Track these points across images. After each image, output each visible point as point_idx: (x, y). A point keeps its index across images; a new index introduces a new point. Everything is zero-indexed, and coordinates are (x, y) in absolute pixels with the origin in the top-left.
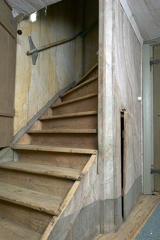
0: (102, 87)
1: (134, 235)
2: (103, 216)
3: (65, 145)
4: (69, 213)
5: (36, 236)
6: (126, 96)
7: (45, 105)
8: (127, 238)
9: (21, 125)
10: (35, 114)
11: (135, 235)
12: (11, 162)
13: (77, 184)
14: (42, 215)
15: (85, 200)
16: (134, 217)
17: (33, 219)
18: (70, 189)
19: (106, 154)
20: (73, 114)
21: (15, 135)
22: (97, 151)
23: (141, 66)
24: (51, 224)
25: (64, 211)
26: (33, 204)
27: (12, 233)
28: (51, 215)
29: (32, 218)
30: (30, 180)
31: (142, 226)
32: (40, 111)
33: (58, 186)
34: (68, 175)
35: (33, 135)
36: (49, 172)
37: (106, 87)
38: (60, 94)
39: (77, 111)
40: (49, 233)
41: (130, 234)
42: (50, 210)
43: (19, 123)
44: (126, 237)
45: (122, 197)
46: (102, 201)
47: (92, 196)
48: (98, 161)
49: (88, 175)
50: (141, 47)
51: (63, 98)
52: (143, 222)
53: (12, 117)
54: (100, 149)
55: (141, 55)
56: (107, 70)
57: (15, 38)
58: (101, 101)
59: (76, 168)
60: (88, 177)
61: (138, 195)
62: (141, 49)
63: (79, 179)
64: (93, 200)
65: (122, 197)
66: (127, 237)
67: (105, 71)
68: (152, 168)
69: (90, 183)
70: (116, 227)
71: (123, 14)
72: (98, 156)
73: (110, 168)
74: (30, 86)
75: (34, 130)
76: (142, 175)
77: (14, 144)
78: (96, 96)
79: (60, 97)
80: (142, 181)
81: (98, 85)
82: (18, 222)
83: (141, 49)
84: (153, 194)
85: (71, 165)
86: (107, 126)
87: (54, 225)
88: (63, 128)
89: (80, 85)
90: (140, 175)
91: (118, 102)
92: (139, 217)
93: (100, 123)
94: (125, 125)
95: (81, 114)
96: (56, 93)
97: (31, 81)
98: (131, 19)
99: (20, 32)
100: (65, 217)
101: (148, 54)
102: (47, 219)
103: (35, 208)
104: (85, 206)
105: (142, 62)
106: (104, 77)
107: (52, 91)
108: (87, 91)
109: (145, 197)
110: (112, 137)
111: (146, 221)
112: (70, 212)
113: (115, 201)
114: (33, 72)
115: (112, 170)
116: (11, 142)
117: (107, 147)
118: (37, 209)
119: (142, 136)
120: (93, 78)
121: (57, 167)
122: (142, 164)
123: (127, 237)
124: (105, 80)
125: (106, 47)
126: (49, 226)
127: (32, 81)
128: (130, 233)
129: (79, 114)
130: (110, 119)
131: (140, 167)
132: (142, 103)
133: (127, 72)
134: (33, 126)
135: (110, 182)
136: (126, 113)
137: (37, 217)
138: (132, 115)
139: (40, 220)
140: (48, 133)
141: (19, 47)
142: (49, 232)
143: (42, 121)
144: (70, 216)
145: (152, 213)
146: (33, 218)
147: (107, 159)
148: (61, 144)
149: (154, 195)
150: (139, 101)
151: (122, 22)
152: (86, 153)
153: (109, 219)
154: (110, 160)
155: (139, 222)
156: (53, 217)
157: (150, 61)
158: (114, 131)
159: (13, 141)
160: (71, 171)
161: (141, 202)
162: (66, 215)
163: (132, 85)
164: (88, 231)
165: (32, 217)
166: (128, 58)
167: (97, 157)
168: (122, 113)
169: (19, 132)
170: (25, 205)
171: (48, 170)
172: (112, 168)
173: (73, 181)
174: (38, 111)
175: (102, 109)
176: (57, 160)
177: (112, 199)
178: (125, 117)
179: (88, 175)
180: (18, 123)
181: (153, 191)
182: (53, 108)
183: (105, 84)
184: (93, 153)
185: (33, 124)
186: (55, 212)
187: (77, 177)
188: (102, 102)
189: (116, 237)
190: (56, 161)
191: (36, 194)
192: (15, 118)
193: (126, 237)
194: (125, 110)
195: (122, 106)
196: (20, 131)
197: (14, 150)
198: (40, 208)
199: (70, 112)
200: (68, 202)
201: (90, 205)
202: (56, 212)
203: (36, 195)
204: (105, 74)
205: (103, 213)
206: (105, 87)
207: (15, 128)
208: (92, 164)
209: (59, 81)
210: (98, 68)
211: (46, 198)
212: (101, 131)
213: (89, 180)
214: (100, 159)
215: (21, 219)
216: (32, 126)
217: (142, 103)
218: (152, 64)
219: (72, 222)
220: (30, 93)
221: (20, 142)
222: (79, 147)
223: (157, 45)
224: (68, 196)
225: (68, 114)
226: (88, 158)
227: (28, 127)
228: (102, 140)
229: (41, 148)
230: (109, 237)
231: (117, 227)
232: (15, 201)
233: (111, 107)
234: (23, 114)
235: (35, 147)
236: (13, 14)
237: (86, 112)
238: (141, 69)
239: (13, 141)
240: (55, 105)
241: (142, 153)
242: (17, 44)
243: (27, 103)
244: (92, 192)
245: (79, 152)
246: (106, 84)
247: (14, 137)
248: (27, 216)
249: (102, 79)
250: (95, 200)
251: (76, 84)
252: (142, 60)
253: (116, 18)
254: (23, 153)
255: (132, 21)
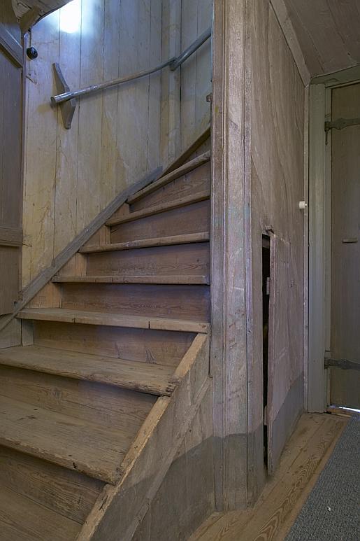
0: (220, 177)
1: (290, 511)
2: (221, 472)
3: (136, 309)
4: (144, 475)
5: (65, 529)
6: (273, 199)
7: (94, 221)
8: (275, 521)
9: (39, 265)
10: (71, 240)
11: (294, 514)
12: (16, 348)
13: (161, 404)
14: (80, 480)
15: (181, 440)
16: (293, 463)
17: (59, 487)
18: (146, 415)
19: (231, 334)
20: (155, 241)
21: (26, 288)
22: (208, 324)
23: (306, 133)
24: (98, 504)
25: (130, 473)
26: (59, 454)
27: (8, 521)
28: (100, 483)
29: (56, 486)
30: (56, 390)
31: (309, 489)
32: (82, 232)
33: (120, 408)
34: (142, 383)
35: (68, 288)
36: (97, 375)
37: (230, 177)
38: (127, 195)
39: (163, 234)
40: (94, 529)
41: (281, 510)
42: (98, 470)
43: (34, 261)
44: (274, 519)
45: (265, 428)
46: (219, 438)
47: (197, 429)
48: (210, 347)
49: (188, 382)
50: (306, 90)
51: (132, 204)
52: (309, 479)
53: (17, 248)
54: (214, 320)
55: (306, 108)
56: (231, 139)
57: (18, 65)
58: (217, 209)
59: (160, 363)
60: (188, 388)
61: (296, 415)
62: (306, 96)
63: (168, 393)
64: (200, 439)
65: (265, 428)
66: (276, 518)
67: (227, 139)
68: (326, 356)
69: (192, 400)
70: (251, 495)
71: (268, 8)
72: (211, 337)
73: (238, 364)
74: (58, 176)
75: (67, 276)
76: (306, 371)
77: (23, 308)
78: (207, 199)
79: (126, 202)
80: (306, 385)
81: (211, 173)
82: (26, 492)
83: (306, 96)
84: (328, 413)
85: (150, 356)
86: (231, 268)
87: (105, 507)
88: (133, 271)
89: (170, 175)
90: (301, 371)
91: (257, 212)
92: (301, 467)
93: (215, 262)
94: (273, 267)
95: (172, 239)
96: (119, 193)
97: (59, 166)
98: (285, 22)
99: (32, 54)
100: (133, 483)
101: (318, 107)
102: (91, 491)
103: (62, 464)
104: (180, 455)
105: (306, 125)
106: (225, 155)
107: (110, 188)
108: (187, 187)
109: (311, 418)
110: (242, 294)
111: (315, 477)
112: (144, 472)
113: (247, 437)
114: (64, 146)
115: (242, 368)
116: (15, 302)
117: (231, 315)
118: (68, 466)
119: (306, 288)
120: (201, 157)
121: (119, 361)
122: (306, 348)
123: (276, 518)
124: (227, 161)
125: (231, 84)
126: (93, 512)
127: (63, 165)
128: (283, 507)
129: (168, 239)
130: (238, 252)
131: (301, 354)
132: (306, 214)
133: (275, 143)
134: (65, 267)
135: (238, 396)
136: (273, 237)
137: (69, 485)
138: (287, 243)
139: (75, 490)
140: (98, 283)
141: (30, 88)
142: (94, 527)
143: (87, 255)
144: (146, 482)
145: (328, 455)
146: (59, 484)
147: (232, 344)
148: (126, 307)
149: (330, 413)
150: (301, 210)
151: (267, 28)
152: (183, 330)
153: (236, 478)
154: (238, 345)
155: (301, 479)
156: (105, 488)
157: (325, 123)
158: (248, 279)
159: (19, 302)
160: (148, 371)
161: (304, 431)
162: (135, 481)
163: (286, 175)
164: (188, 509)
165: (56, 483)
166: (278, 113)
167: (208, 341)
168: (266, 238)
169: (33, 281)
170: (40, 456)
171: (96, 371)
172: (241, 366)
173: (155, 396)
174: (78, 232)
175: (220, 229)
176: (118, 345)
177: (241, 435)
178: (273, 248)
179: (188, 382)
180: (31, 261)
181: (329, 404)
182: (112, 227)
183: (227, 171)
184: (199, 331)
185: (67, 263)
186: (109, 475)
187: (162, 387)
188: (220, 213)
189: (251, 519)
190: (116, 347)
191: (68, 424)
192: (25, 250)
193: (274, 519)
194: (271, 230)
195: (266, 222)
196: (37, 277)
197: (22, 320)
198: (74, 464)
199: (146, 235)
200: (141, 450)
201: (192, 451)
202: (111, 475)
203: (68, 427)
204: (227, 146)
205: (223, 465)
206: (227, 177)
207: (25, 272)
208: (197, 356)
209: (126, 166)
210: (210, 135)
211: (90, 437)
212: (219, 279)
213: (189, 393)
214: (215, 344)
215: (32, 486)
216: (64, 266)
217: (306, 214)
218: (330, 129)
219: (150, 494)
220: (58, 193)
221: (38, 303)
222: (168, 314)
223: (340, 87)
224: (142, 434)
225: (143, 240)
226: (189, 344)
227: (55, 270)
228: (220, 302)
229: (82, 318)
230: (234, 520)
231: (253, 496)
232: (18, 444)
233: (240, 223)
234: (43, 239)
235: (68, 315)
236: (15, 10)
237: (183, 236)
238: (306, 140)
239: (19, 302)
240: (114, 221)
241: (306, 324)
242: (27, 80)
243: (53, 217)
244: (198, 420)
245: (167, 329)
246: (230, 171)
247: (21, 293)
248: (44, 480)
249: (220, 158)
250: (203, 438)
251: (162, 174)
252: (306, 119)
253: (252, 15)
254: (43, 328)
255: (288, 27)
